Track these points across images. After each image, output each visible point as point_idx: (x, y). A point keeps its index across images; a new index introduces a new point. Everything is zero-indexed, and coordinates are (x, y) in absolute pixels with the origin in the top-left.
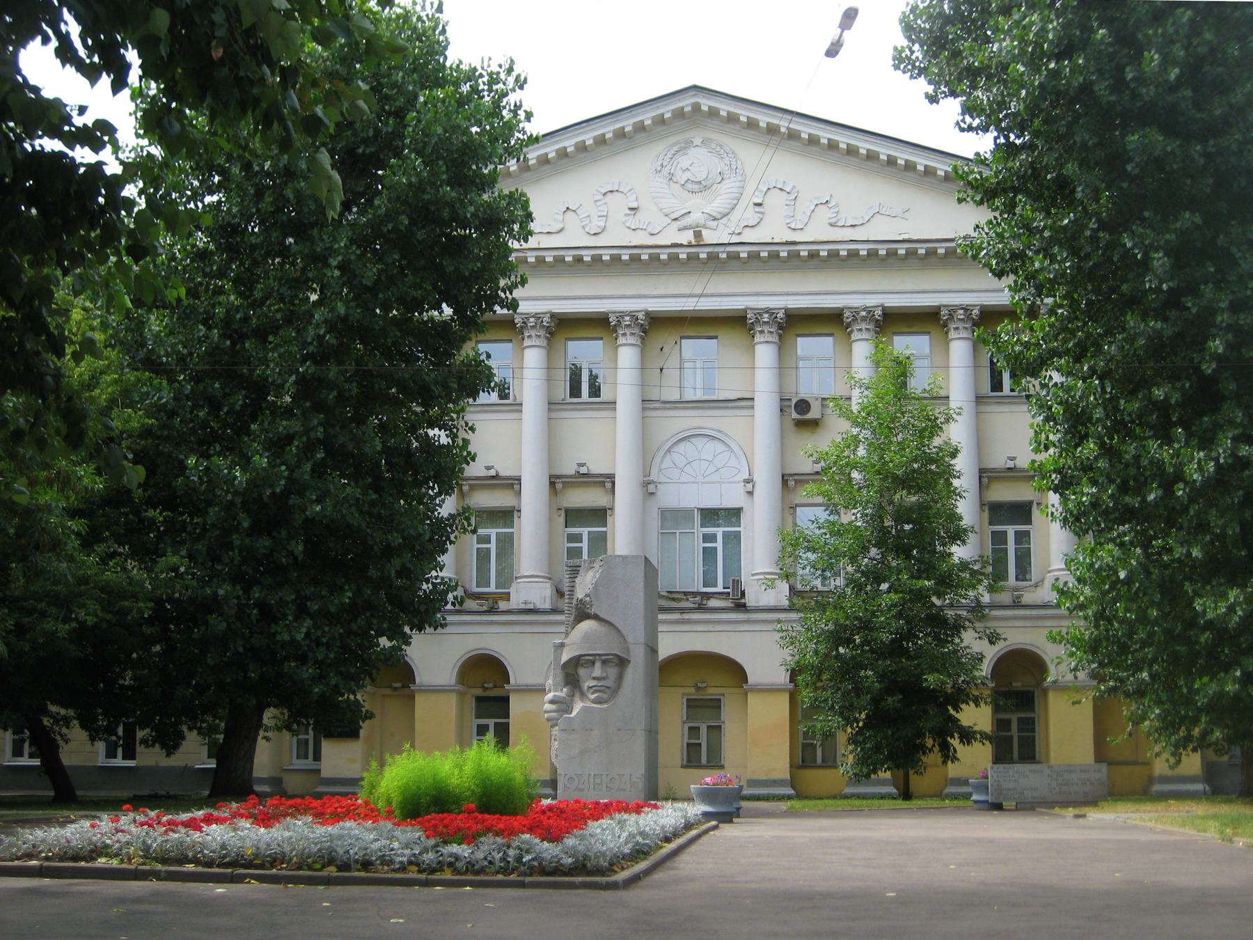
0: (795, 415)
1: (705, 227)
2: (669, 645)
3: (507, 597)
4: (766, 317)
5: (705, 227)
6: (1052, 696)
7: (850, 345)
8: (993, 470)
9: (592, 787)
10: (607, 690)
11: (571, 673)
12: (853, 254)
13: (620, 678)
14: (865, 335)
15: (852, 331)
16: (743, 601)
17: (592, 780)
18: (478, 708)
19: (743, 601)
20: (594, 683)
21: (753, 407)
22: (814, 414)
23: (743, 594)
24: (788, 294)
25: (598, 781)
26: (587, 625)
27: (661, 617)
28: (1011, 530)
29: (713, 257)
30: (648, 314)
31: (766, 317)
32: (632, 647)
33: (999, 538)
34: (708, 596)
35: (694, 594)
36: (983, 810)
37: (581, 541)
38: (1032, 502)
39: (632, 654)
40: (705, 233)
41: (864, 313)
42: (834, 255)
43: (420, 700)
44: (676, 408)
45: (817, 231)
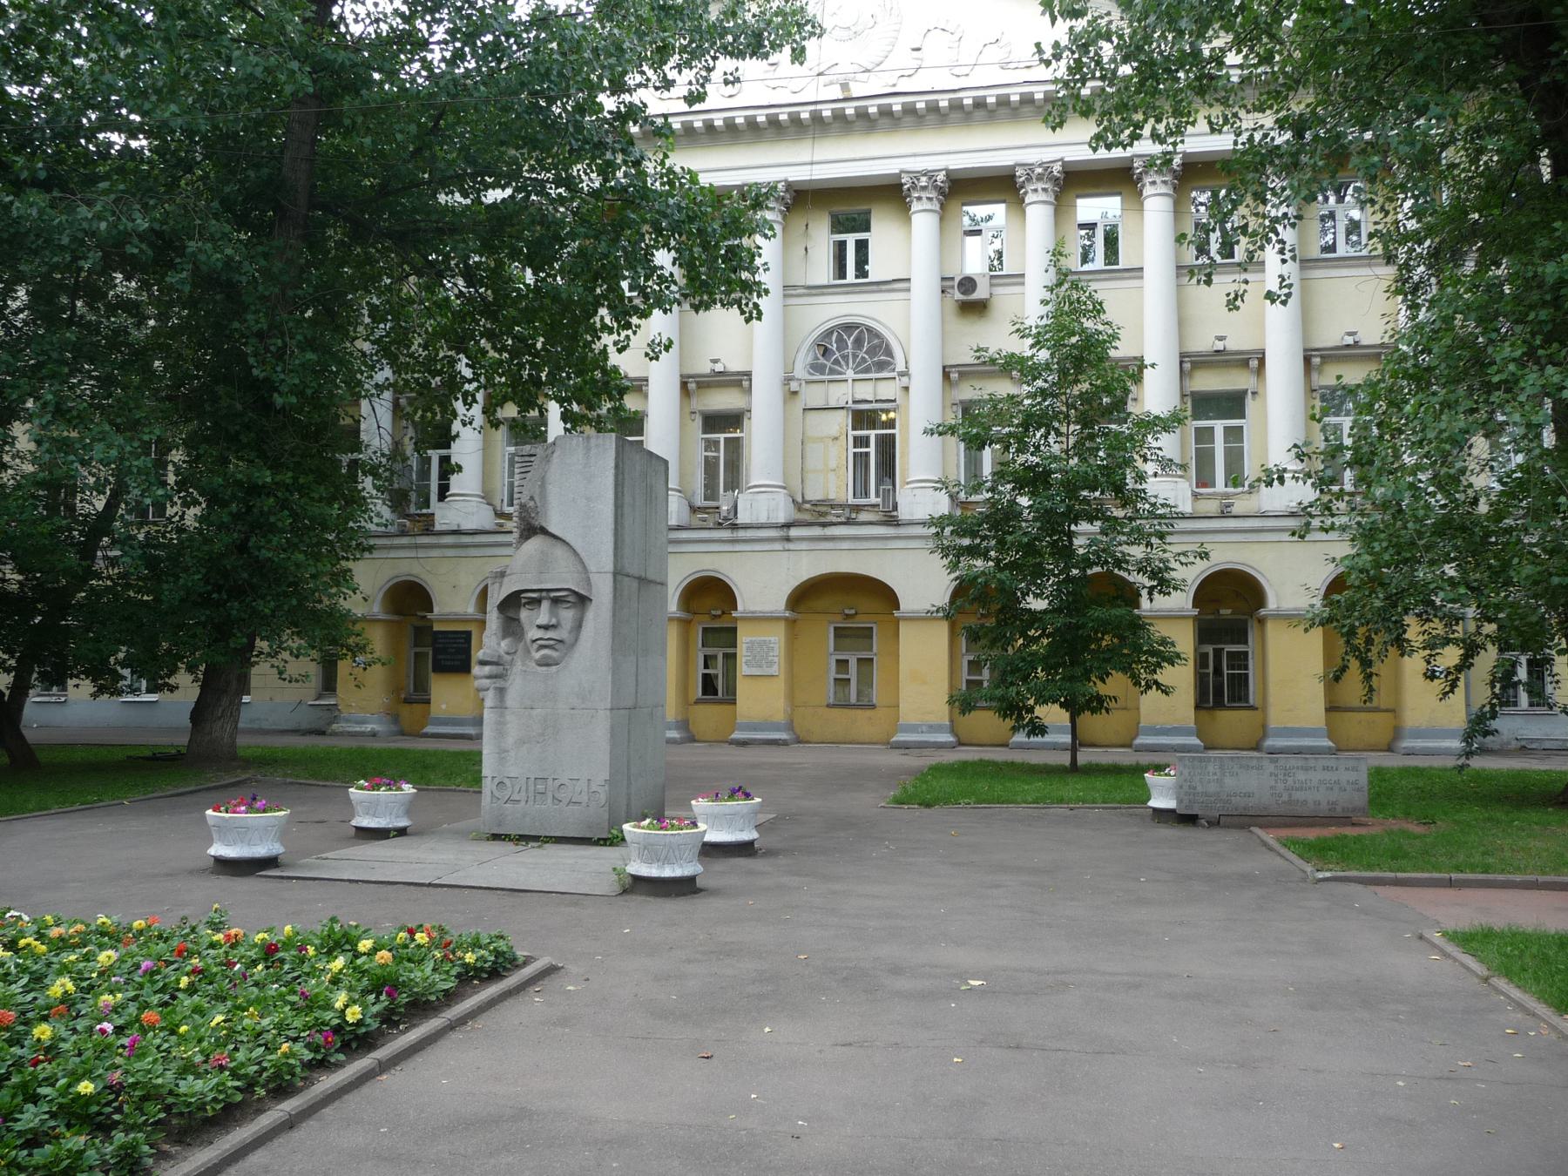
0: (958, 296)
4: (924, 181)
6: (1270, 626)
7: (1024, 212)
9: (531, 794)
10: (558, 646)
13: (578, 626)
14: (1042, 197)
15: (1026, 193)
16: (895, 513)
17: (532, 788)
19: (895, 513)
20: (539, 634)
21: (908, 290)
22: (980, 293)
23: (895, 508)
24: (915, 155)
25: (540, 787)
26: (535, 544)
28: (1219, 426)
29: (862, 114)
30: (789, 186)
31: (924, 181)
32: (594, 578)
33: (1204, 435)
34: (857, 508)
37: (867, 446)
38: (1245, 392)
39: (594, 590)
40: (852, 85)
41: (1040, 170)
43: (903, 627)
44: (823, 294)
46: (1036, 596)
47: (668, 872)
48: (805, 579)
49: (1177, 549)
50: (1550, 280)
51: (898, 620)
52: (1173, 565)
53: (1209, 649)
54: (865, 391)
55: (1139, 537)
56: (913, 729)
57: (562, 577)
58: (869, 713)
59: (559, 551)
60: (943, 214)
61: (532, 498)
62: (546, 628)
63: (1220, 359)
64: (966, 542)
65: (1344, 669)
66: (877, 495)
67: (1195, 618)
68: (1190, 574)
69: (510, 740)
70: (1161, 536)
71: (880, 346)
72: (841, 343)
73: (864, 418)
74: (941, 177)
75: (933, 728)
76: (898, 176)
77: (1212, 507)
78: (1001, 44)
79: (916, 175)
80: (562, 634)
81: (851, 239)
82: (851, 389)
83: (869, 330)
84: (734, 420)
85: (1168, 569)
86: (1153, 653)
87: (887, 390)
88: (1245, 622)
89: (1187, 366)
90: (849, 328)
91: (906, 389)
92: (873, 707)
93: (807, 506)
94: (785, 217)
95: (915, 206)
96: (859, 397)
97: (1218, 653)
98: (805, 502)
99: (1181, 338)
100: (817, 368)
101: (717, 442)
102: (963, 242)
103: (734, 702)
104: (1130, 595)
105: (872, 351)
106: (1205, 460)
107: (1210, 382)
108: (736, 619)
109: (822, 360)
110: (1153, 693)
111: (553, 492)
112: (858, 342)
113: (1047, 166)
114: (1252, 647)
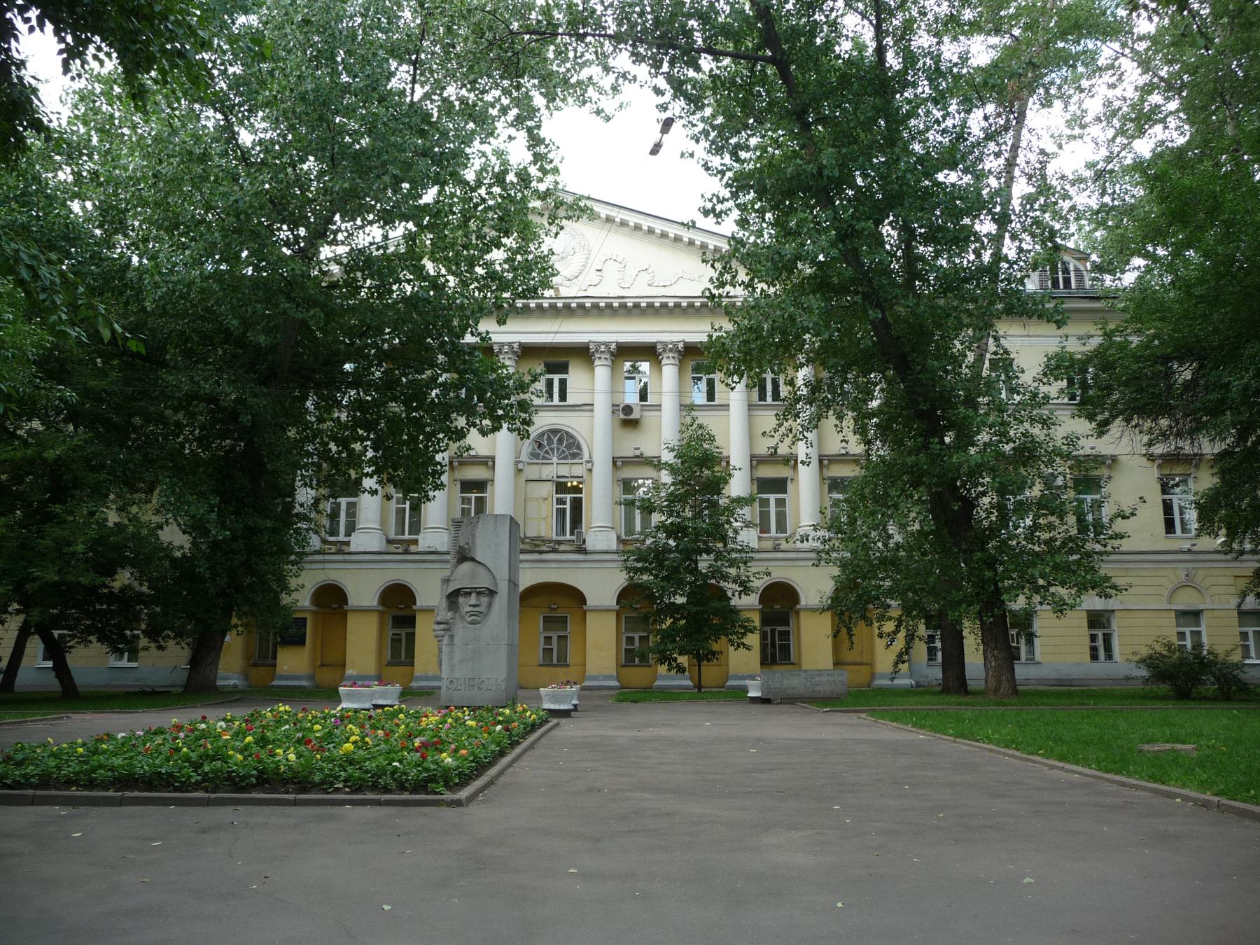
0: (622, 416)
1: (561, 285)
2: (528, 579)
3: (416, 542)
4: (603, 348)
5: (561, 285)
8: (761, 456)
11: (453, 598)
12: (664, 305)
13: (490, 605)
14: (672, 361)
18: (393, 622)
21: (592, 411)
22: (635, 415)
23: (584, 541)
24: (598, 332)
25: (472, 683)
26: (466, 566)
27: (523, 557)
28: (772, 498)
29: (567, 307)
30: (520, 344)
31: (603, 348)
33: (765, 503)
34: (559, 543)
35: (550, 541)
36: (1164, 698)
42: (650, 305)
43: (590, 618)
45: (639, 289)
46: (681, 595)
47: (562, 707)
48: (576, 586)
49: (753, 570)
50: (910, 464)
51: (585, 612)
52: (752, 579)
53: (768, 629)
54: (564, 470)
55: (733, 563)
56: (595, 678)
57: (483, 582)
58: (565, 670)
59: (481, 570)
60: (614, 367)
61: (467, 544)
62: (474, 606)
63: (773, 458)
64: (640, 565)
65: (838, 631)
66: (572, 534)
67: (760, 610)
68: (759, 584)
69: (456, 661)
70: (745, 563)
71: (574, 443)
72: (550, 441)
73: (561, 487)
74: (613, 346)
75: (606, 678)
76: (588, 343)
77: (768, 545)
78: (650, 271)
79: (599, 344)
80: (482, 609)
81: (556, 378)
82: (555, 468)
83: (567, 433)
84: (480, 486)
85: (749, 581)
86: (742, 627)
87: (578, 470)
88: (788, 614)
89: (755, 463)
90: (555, 432)
91: (590, 470)
92: (568, 666)
93: (528, 540)
94: (517, 362)
95: (597, 362)
96: (560, 474)
97: (773, 631)
98: (526, 538)
99: (751, 446)
100: (534, 455)
101: (470, 499)
102: (624, 383)
103: (412, 664)
104: (722, 595)
105: (569, 447)
106: (764, 516)
107: (767, 472)
108: (415, 611)
109: (538, 451)
110: (741, 650)
111: (478, 541)
112: (560, 441)
113: (675, 344)
114: (792, 628)
